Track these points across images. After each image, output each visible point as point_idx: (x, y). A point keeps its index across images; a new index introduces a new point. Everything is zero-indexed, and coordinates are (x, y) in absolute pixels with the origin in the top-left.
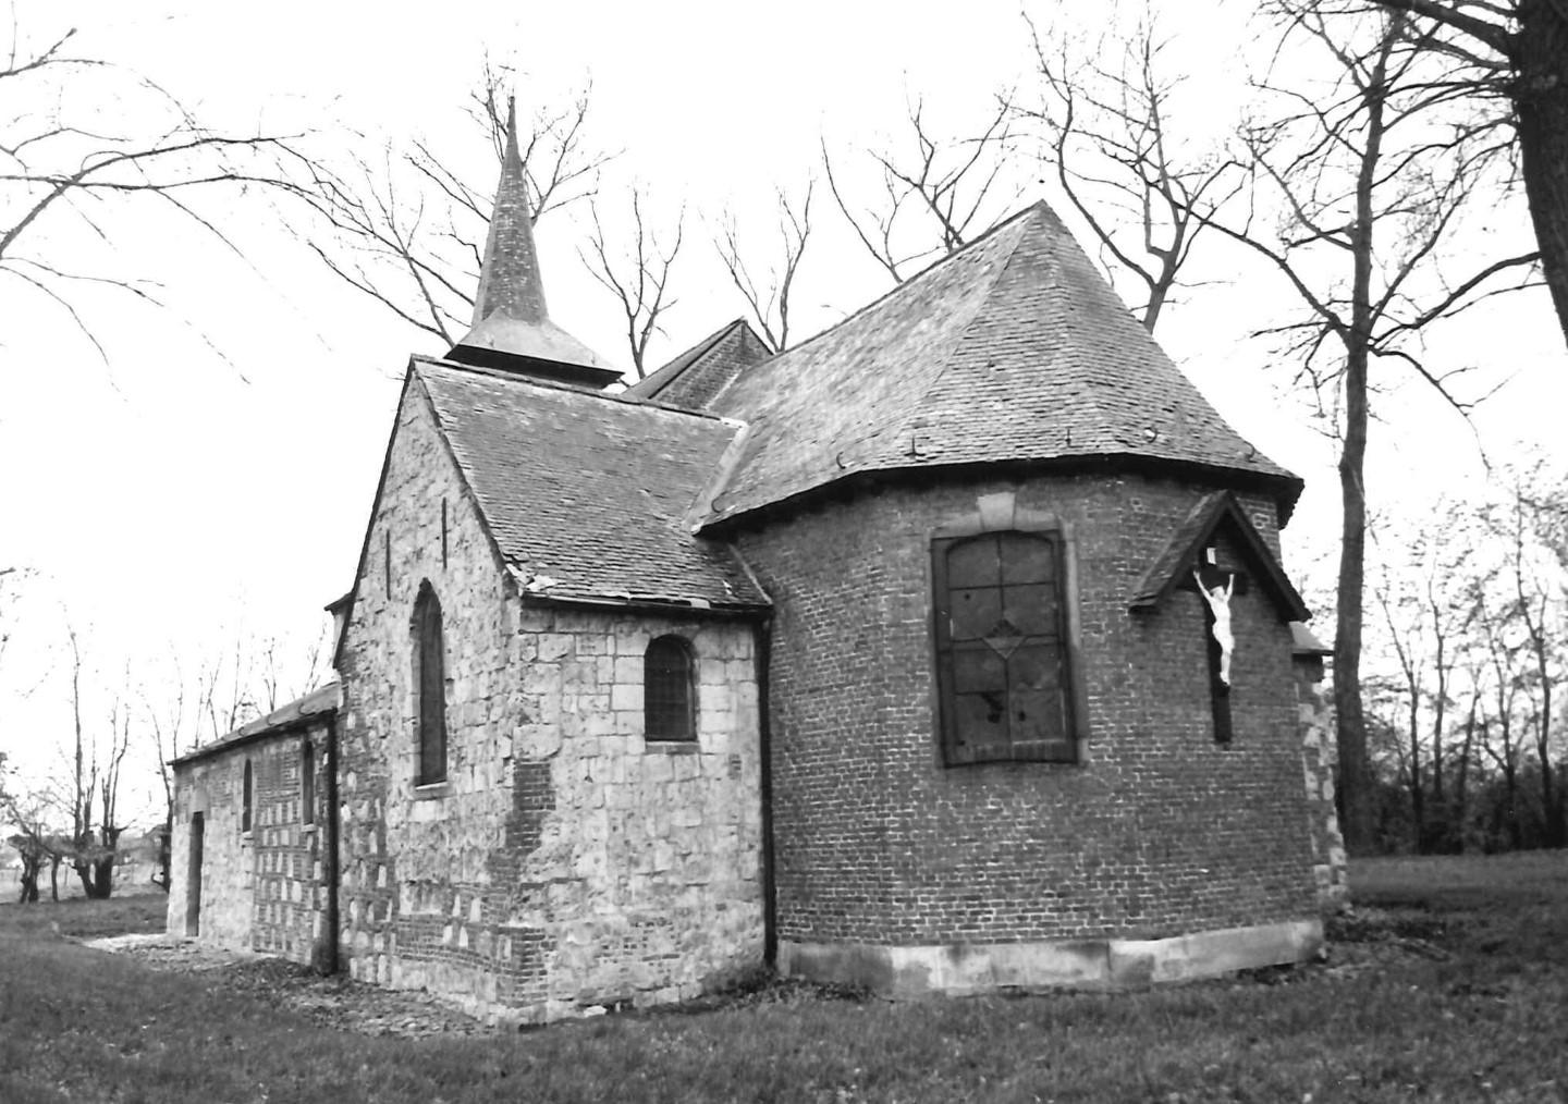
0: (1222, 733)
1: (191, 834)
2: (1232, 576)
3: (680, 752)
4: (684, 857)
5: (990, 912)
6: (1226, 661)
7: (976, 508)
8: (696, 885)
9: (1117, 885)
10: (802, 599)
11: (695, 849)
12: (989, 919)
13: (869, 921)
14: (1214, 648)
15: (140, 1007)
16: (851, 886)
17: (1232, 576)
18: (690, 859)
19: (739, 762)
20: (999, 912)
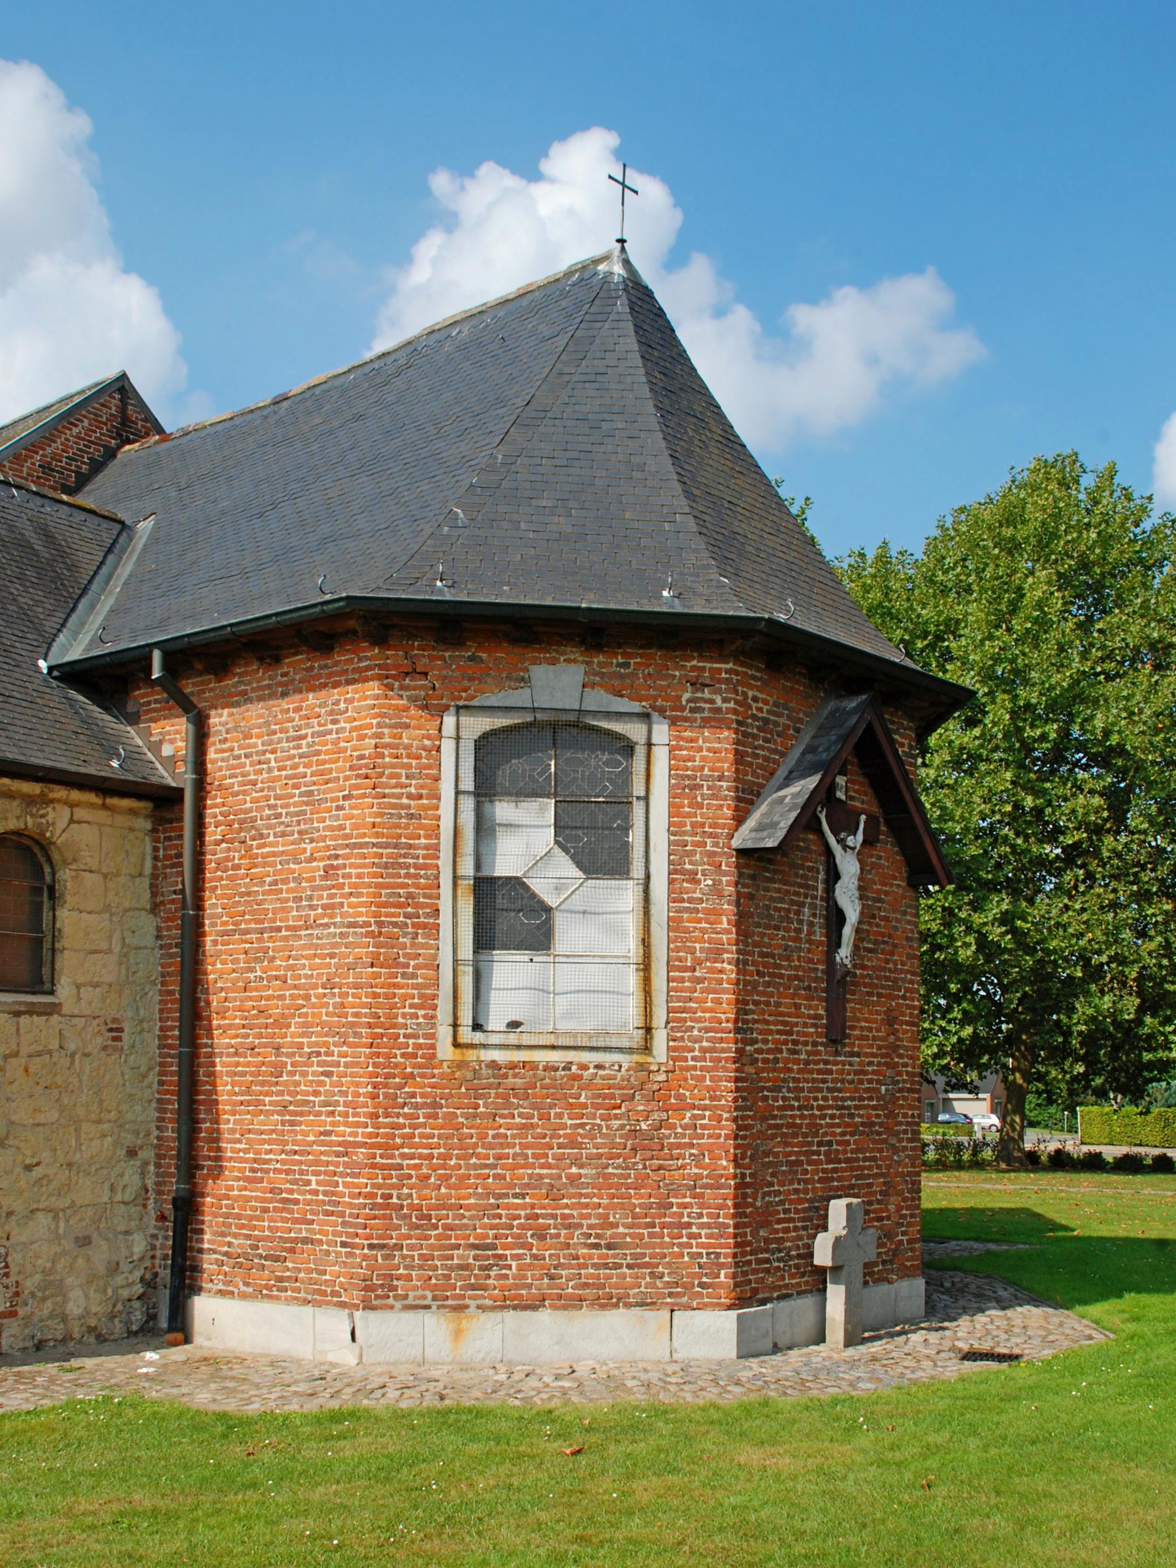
0: (836, 1035)
1: (553, 662)
2: (863, 817)
3: (32, 1010)
4: (28, 1168)
5: (509, 1267)
6: (848, 931)
7: (525, 681)
8: (47, 1210)
9: (691, 1236)
10: (237, 794)
11: (45, 1156)
12: (506, 1277)
13: (324, 1272)
14: (836, 918)
15: (1039, 891)
16: (296, 1221)
17: (863, 817)
18: (37, 1172)
19: (120, 1030)
20: (519, 1268)
